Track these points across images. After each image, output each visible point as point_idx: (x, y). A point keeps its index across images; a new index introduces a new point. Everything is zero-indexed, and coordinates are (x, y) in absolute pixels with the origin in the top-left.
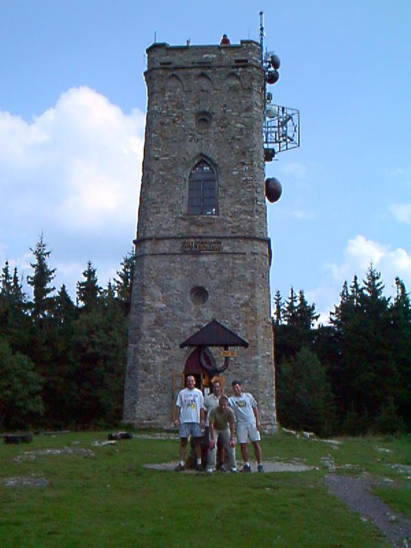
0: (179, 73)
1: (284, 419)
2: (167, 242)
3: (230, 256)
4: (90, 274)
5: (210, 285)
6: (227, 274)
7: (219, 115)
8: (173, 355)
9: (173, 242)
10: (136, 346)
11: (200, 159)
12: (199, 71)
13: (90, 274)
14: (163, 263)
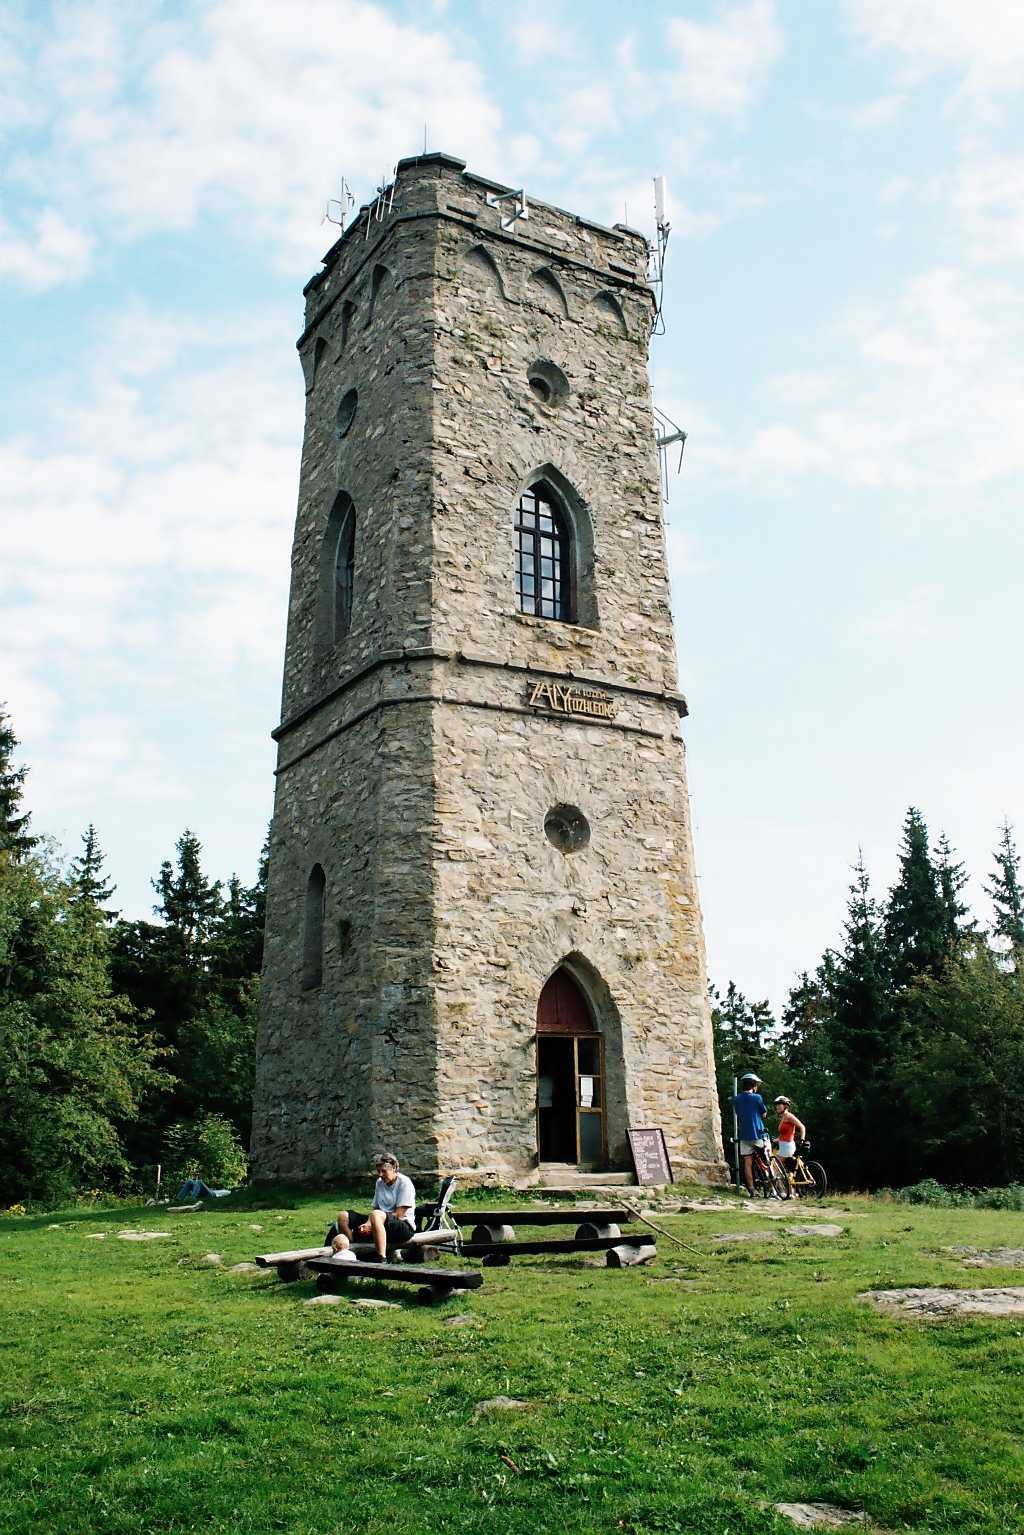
0: (497, 250)
1: (330, 1245)
2: (490, 678)
3: (631, 736)
4: (189, 852)
5: (591, 807)
6: (627, 783)
7: (579, 383)
8: (520, 984)
9: (503, 678)
10: (418, 953)
11: (541, 478)
12: (541, 263)
13: (189, 852)
14: (481, 730)
